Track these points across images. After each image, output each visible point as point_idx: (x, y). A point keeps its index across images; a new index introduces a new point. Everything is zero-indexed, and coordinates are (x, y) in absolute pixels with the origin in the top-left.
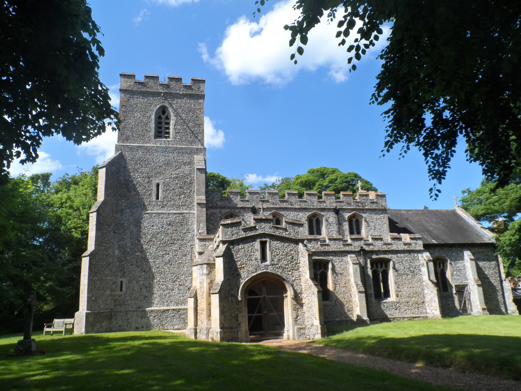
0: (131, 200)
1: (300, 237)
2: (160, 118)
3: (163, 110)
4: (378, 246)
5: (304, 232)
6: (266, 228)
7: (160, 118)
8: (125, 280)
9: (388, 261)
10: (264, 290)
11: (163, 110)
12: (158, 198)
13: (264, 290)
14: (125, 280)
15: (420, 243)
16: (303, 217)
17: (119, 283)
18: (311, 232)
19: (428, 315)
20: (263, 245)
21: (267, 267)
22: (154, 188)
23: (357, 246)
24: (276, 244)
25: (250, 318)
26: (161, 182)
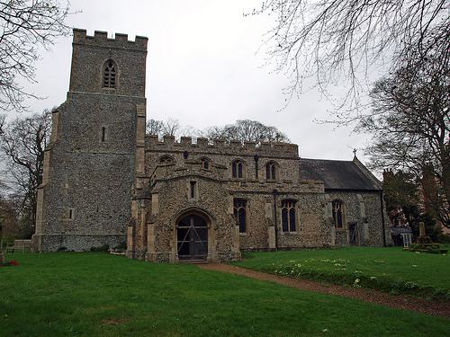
0: (214, 315)
1: (224, 179)
2: (107, 70)
3: (110, 63)
4: (288, 188)
5: (229, 174)
6: (196, 170)
7: (107, 70)
8: (73, 210)
9: (294, 202)
10: (192, 221)
11: (110, 63)
12: (103, 140)
13: (192, 221)
14: (73, 210)
15: (323, 187)
16: (227, 162)
17: (69, 212)
18: (234, 175)
19: (437, 290)
20: (193, 183)
21: (194, 202)
22: (100, 133)
23: (272, 187)
24: (204, 183)
25: (179, 244)
26: (106, 127)
